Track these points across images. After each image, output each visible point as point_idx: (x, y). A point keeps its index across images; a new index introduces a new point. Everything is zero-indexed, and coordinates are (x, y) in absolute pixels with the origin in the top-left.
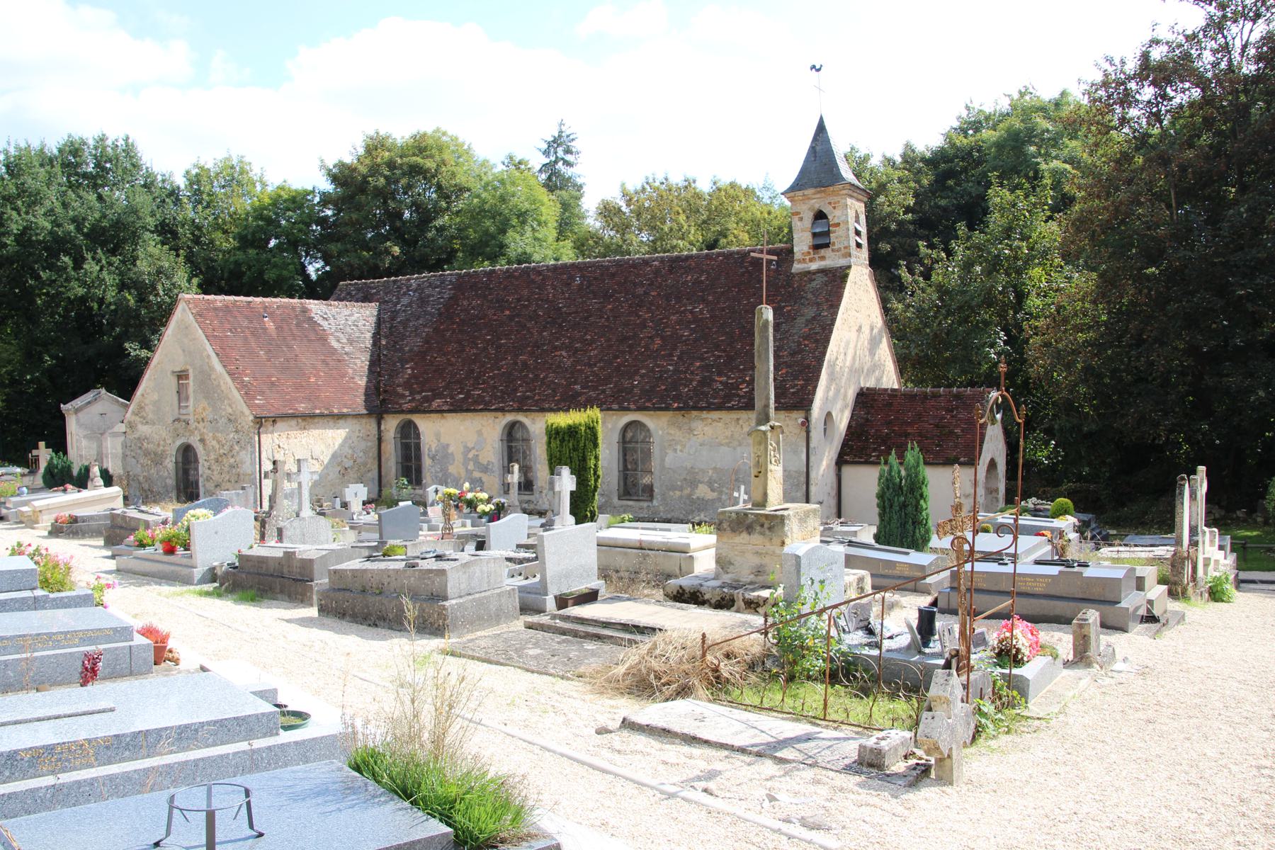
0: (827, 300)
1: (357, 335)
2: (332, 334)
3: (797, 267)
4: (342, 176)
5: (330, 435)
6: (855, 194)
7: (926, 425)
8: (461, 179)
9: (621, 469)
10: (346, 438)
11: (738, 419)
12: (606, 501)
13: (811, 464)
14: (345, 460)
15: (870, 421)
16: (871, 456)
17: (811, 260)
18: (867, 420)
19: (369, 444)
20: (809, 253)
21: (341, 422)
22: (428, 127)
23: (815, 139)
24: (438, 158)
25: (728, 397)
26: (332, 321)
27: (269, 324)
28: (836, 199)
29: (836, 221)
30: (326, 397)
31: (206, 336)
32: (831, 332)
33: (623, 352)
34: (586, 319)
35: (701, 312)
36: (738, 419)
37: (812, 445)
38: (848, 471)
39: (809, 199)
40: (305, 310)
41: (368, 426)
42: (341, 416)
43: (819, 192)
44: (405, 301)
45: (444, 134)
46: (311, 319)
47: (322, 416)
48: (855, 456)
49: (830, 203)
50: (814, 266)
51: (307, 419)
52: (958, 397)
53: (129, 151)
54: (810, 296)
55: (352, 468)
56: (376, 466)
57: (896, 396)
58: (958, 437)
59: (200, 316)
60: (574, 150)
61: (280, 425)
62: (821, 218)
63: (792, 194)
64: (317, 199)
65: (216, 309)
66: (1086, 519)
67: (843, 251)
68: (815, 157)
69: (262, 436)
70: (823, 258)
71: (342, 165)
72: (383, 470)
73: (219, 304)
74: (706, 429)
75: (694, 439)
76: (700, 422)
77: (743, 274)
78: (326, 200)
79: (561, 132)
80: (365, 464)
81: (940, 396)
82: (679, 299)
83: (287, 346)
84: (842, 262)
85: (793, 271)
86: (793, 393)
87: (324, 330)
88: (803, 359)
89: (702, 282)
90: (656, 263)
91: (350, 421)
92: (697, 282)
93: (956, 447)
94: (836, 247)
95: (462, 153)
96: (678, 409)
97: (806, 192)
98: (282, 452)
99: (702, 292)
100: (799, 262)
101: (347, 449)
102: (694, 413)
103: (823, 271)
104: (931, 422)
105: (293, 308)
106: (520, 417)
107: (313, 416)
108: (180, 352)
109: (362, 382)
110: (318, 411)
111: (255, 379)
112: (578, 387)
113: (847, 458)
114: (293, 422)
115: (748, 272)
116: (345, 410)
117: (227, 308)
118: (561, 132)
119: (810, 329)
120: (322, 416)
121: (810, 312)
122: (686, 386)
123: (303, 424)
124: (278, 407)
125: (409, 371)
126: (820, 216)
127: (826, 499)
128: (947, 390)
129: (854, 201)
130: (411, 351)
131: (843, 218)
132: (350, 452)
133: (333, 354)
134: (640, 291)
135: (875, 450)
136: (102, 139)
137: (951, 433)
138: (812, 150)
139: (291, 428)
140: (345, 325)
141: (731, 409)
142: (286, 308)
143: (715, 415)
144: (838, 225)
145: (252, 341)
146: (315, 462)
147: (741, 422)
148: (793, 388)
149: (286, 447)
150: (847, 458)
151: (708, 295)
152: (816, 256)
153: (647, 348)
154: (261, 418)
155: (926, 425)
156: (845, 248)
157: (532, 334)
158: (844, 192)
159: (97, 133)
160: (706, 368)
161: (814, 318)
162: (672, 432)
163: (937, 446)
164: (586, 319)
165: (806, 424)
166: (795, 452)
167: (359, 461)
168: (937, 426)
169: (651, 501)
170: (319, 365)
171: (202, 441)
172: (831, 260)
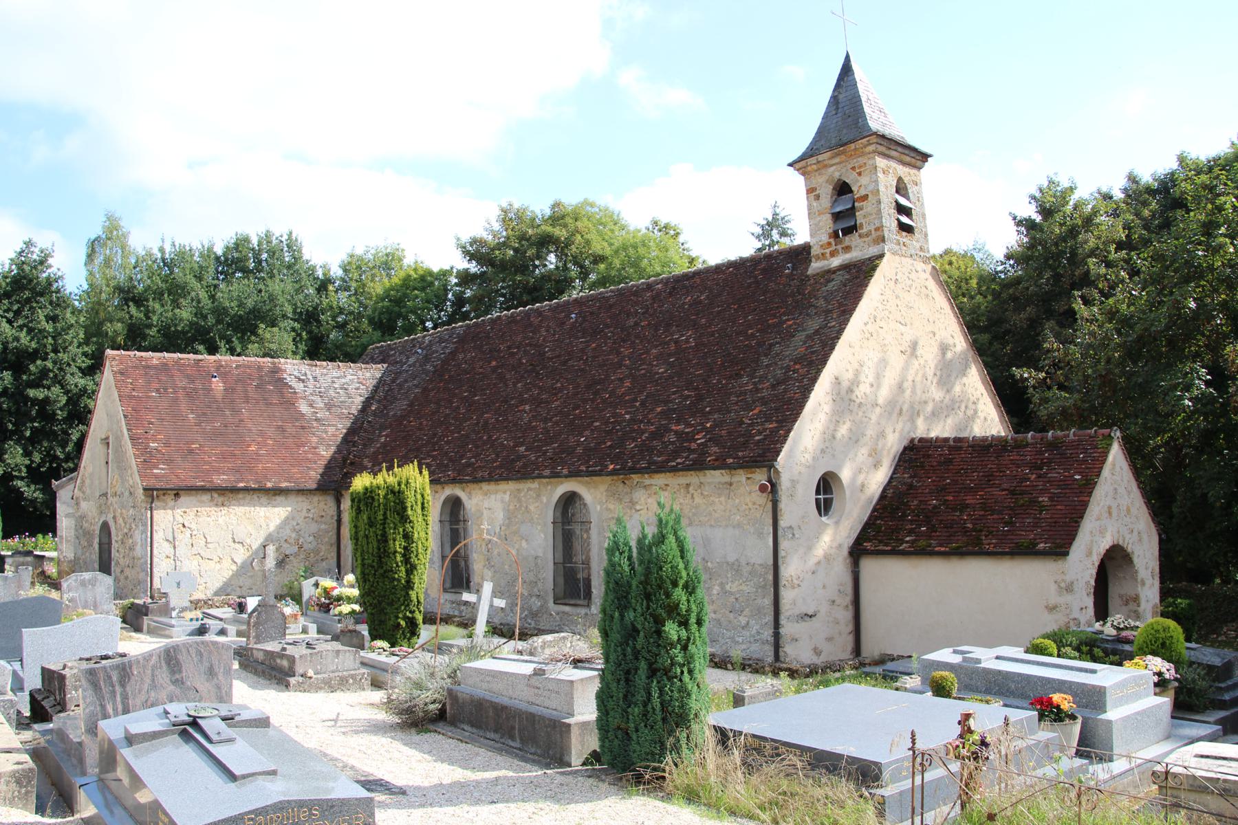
0: (841, 305)
1: (342, 399)
2: (305, 398)
3: (815, 266)
4: (475, 252)
5: (262, 514)
6: (893, 153)
7: (996, 492)
8: (598, 247)
9: (560, 559)
10: (287, 518)
11: (688, 485)
12: (542, 606)
13: (782, 553)
14: (285, 545)
15: (916, 488)
16: (903, 542)
17: (833, 254)
18: (911, 486)
19: (323, 526)
20: (829, 244)
21: (279, 499)
22: (571, 199)
23: (838, 86)
24: (572, 227)
25: (675, 454)
26: (311, 384)
27: (218, 385)
28: (861, 160)
29: (863, 192)
30: (264, 468)
31: (120, 396)
32: (832, 348)
33: (585, 401)
34: (565, 363)
35: (687, 341)
36: (688, 485)
37: (783, 523)
38: (872, 568)
39: (826, 166)
40: (276, 370)
41: (322, 505)
42: (278, 492)
43: (837, 155)
44: (412, 360)
45: (592, 205)
46: (281, 380)
47: (247, 490)
48: (880, 542)
49: (853, 168)
50: (836, 262)
51: (227, 493)
52: (1054, 445)
53: (293, 245)
54: (822, 302)
55: (296, 555)
56: (334, 554)
57: (960, 448)
58: (1042, 508)
59: (122, 374)
60: (789, 232)
61: (184, 499)
62: (845, 193)
63: (803, 163)
64: (454, 280)
65: (148, 367)
66: (1217, 661)
67: (874, 234)
68: (837, 108)
69: (155, 512)
70: (847, 249)
71: (474, 241)
72: (342, 559)
73: (155, 362)
74: (649, 500)
75: (636, 516)
76: (643, 491)
77: (749, 286)
78: (466, 278)
79: (775, 214)
80: (317, 552)
81: (1027, 445)
82: (668, 325)
83: (233, 410)
84: (873, 251)
85: (810, 272)
86: (759, 441)
87: (295, 393)
88: (785, 391)
89: (700, 302)
90: (660, 286)
91: (293, 498)
92: (697, 302)
93: (1036, 525)
94: (864, 231)
95: (610, 221)
96: (614, 473)
97: (820, 158)
98: (188, 532)
99: (697, 315)
100: (818, 258)
101: (288, 531)
102: (636, 478)
103: (845, 267)
104: (1005, 486)
105: (260, 368)
106: (458, 491)
107: (234, 490)
108: (106, 416)
109: (326, 453)
110: (241, 485)
111: (167, 445)
112: (522, 449)
113: (867, 545)
114: (206, 497)
115: (757, 282)
116: (284, 485)
117: (164, 367)
118: (775, 214)
119: (807, 349)
120: (247, 490)
121: (813, 324)
122: (634, 439)
123: (221, 499)
124: (185, 475)
125: (383, 439)
126: (843, 189)
127: (824, 609)
128: (1039, 435)
129: (893, 164)
130: (393, 415)
131: (871, 187)
132: (294, 535)
133: (297, 420)
134: (631, 322)
135: (910, 532)
136: (268, 235)
137: (1034, 502)
138: (835, 100)
139: (202, 503)
140: (328, 389)
141: (674, 470)
142: (249, 367)
143: (660, 480)
144: (865, 197)
145: (183, 405)
146: (237, 546)
147: (691, 489)
148: (760, 433)
149: (193, 526)
150: (867, 545)
151: (702, 318)
152: (839, 247)
153: (612, 393)
154: (152, 490)
155: (996, 492)
156: (877, 229)
157: (507, 386)
158: (871, 148)
159: (262, 231)
160: (665, 414)
161: (817, 332)
162: (611, 506)
163: (1006, 524)
164: (565, 363)
165: (772, 489)
166: (760, 535)
167: (306, 546)
168: (1012, 492)
169: (588, 606)
170: (271, 432)
171: (114, 518)
172: (859, 250)
